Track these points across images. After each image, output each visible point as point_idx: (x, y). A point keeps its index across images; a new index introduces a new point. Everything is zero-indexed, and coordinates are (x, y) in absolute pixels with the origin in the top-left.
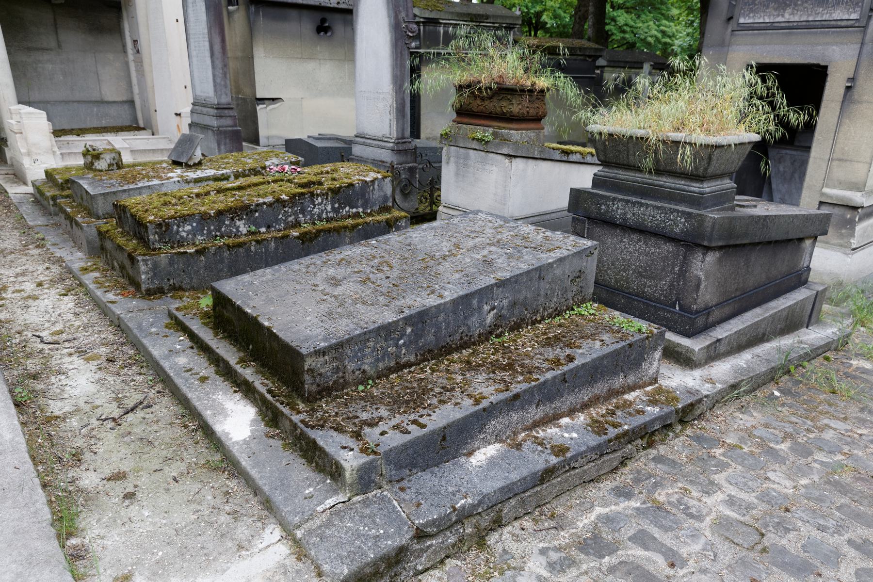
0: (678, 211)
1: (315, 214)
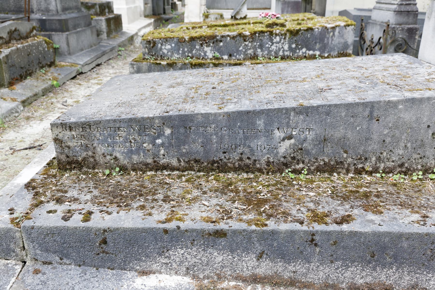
1: (272, 51)
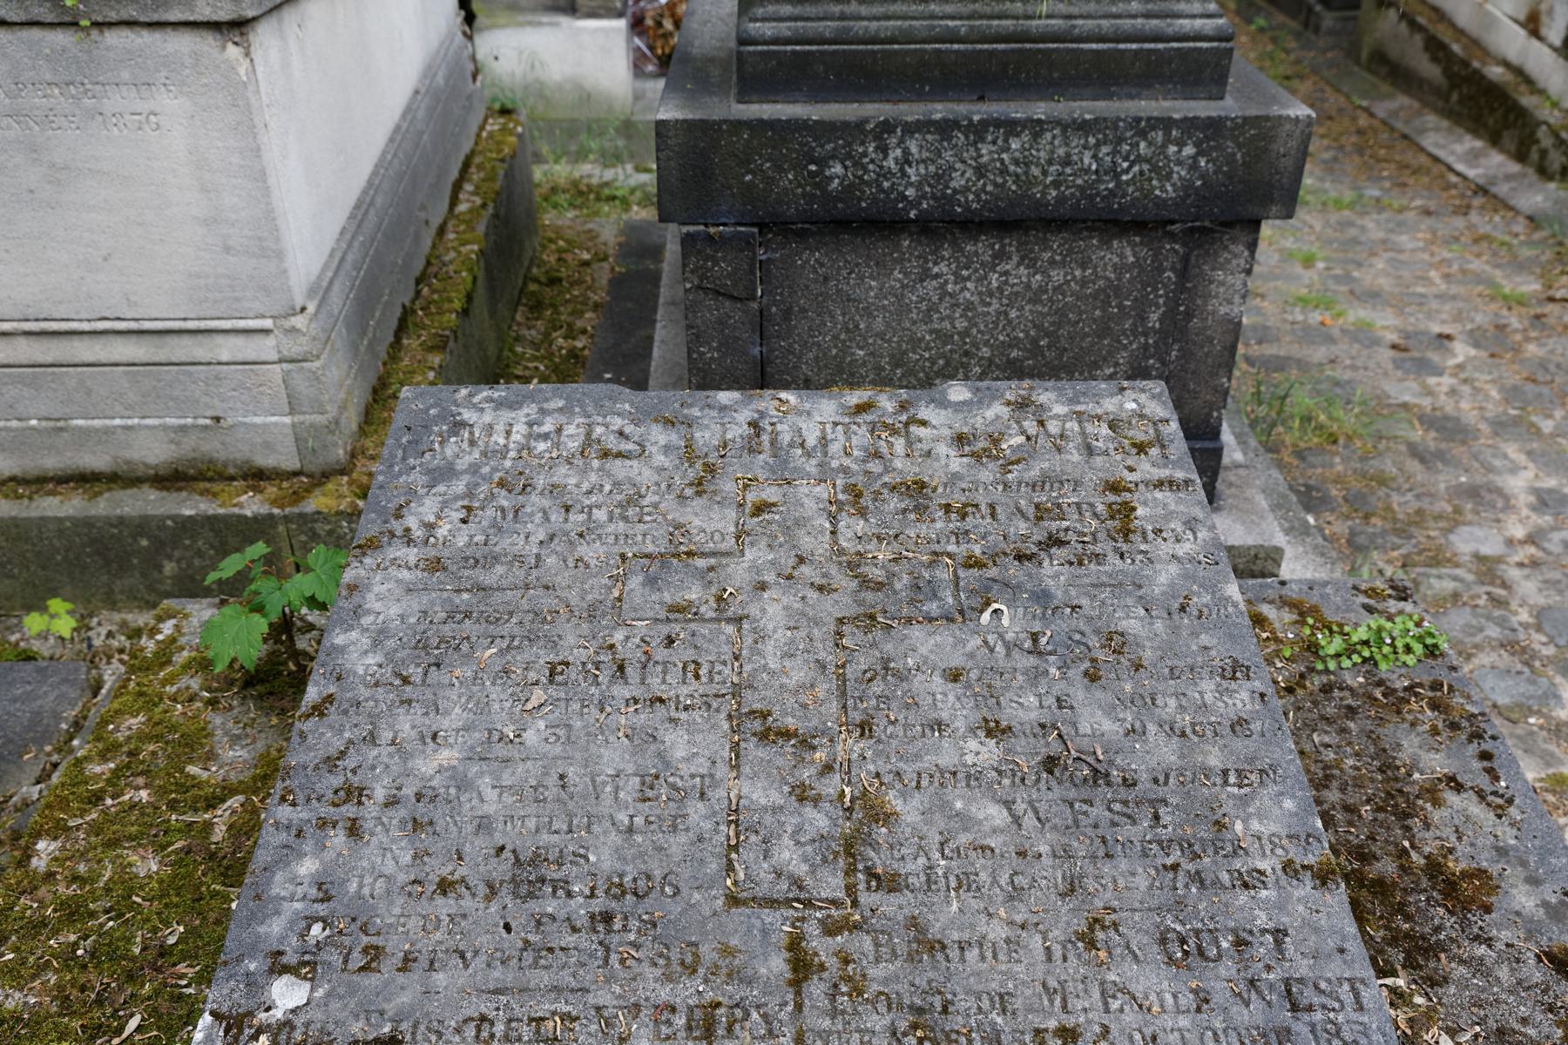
0: (1166, 123)
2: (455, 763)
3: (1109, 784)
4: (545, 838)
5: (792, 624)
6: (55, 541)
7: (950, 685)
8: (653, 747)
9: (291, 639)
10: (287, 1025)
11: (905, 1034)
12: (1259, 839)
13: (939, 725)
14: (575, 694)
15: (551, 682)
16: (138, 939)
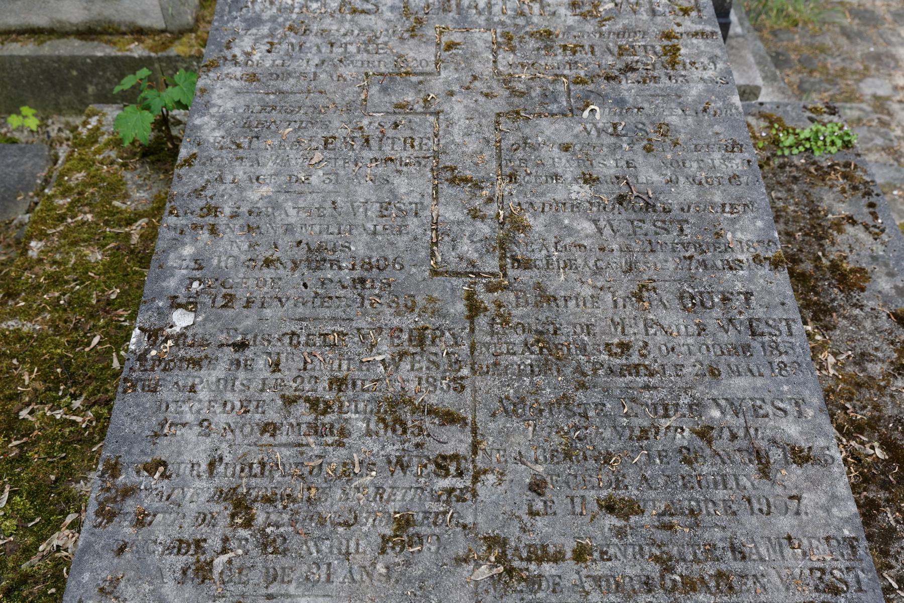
2: (271, 194)
3: (655, 211)
4: (325, 237)
5: (469, 116)
6: (21, 71)
7: (563, 153)
8: (387, 187)
9: (168, 129)
10: (183, 335)
11: (532, 345)
12: (741, 243)
13: (556, 176)
14: (340, 155)
15: (326, 148)
16: (94, 296)
